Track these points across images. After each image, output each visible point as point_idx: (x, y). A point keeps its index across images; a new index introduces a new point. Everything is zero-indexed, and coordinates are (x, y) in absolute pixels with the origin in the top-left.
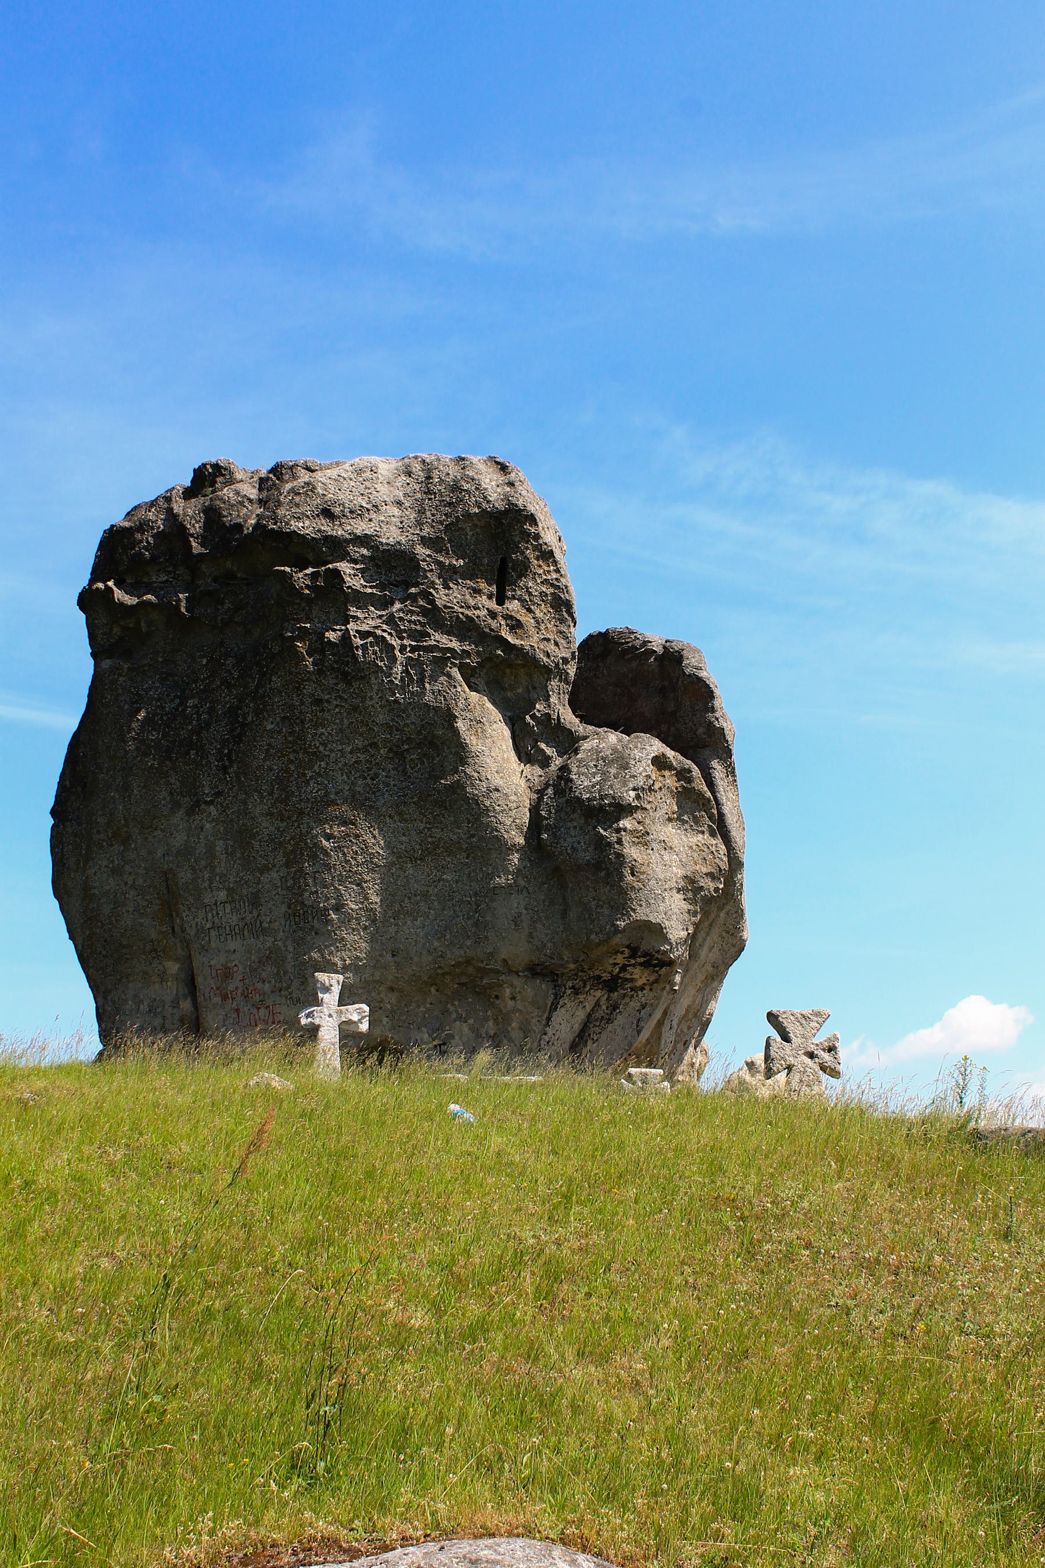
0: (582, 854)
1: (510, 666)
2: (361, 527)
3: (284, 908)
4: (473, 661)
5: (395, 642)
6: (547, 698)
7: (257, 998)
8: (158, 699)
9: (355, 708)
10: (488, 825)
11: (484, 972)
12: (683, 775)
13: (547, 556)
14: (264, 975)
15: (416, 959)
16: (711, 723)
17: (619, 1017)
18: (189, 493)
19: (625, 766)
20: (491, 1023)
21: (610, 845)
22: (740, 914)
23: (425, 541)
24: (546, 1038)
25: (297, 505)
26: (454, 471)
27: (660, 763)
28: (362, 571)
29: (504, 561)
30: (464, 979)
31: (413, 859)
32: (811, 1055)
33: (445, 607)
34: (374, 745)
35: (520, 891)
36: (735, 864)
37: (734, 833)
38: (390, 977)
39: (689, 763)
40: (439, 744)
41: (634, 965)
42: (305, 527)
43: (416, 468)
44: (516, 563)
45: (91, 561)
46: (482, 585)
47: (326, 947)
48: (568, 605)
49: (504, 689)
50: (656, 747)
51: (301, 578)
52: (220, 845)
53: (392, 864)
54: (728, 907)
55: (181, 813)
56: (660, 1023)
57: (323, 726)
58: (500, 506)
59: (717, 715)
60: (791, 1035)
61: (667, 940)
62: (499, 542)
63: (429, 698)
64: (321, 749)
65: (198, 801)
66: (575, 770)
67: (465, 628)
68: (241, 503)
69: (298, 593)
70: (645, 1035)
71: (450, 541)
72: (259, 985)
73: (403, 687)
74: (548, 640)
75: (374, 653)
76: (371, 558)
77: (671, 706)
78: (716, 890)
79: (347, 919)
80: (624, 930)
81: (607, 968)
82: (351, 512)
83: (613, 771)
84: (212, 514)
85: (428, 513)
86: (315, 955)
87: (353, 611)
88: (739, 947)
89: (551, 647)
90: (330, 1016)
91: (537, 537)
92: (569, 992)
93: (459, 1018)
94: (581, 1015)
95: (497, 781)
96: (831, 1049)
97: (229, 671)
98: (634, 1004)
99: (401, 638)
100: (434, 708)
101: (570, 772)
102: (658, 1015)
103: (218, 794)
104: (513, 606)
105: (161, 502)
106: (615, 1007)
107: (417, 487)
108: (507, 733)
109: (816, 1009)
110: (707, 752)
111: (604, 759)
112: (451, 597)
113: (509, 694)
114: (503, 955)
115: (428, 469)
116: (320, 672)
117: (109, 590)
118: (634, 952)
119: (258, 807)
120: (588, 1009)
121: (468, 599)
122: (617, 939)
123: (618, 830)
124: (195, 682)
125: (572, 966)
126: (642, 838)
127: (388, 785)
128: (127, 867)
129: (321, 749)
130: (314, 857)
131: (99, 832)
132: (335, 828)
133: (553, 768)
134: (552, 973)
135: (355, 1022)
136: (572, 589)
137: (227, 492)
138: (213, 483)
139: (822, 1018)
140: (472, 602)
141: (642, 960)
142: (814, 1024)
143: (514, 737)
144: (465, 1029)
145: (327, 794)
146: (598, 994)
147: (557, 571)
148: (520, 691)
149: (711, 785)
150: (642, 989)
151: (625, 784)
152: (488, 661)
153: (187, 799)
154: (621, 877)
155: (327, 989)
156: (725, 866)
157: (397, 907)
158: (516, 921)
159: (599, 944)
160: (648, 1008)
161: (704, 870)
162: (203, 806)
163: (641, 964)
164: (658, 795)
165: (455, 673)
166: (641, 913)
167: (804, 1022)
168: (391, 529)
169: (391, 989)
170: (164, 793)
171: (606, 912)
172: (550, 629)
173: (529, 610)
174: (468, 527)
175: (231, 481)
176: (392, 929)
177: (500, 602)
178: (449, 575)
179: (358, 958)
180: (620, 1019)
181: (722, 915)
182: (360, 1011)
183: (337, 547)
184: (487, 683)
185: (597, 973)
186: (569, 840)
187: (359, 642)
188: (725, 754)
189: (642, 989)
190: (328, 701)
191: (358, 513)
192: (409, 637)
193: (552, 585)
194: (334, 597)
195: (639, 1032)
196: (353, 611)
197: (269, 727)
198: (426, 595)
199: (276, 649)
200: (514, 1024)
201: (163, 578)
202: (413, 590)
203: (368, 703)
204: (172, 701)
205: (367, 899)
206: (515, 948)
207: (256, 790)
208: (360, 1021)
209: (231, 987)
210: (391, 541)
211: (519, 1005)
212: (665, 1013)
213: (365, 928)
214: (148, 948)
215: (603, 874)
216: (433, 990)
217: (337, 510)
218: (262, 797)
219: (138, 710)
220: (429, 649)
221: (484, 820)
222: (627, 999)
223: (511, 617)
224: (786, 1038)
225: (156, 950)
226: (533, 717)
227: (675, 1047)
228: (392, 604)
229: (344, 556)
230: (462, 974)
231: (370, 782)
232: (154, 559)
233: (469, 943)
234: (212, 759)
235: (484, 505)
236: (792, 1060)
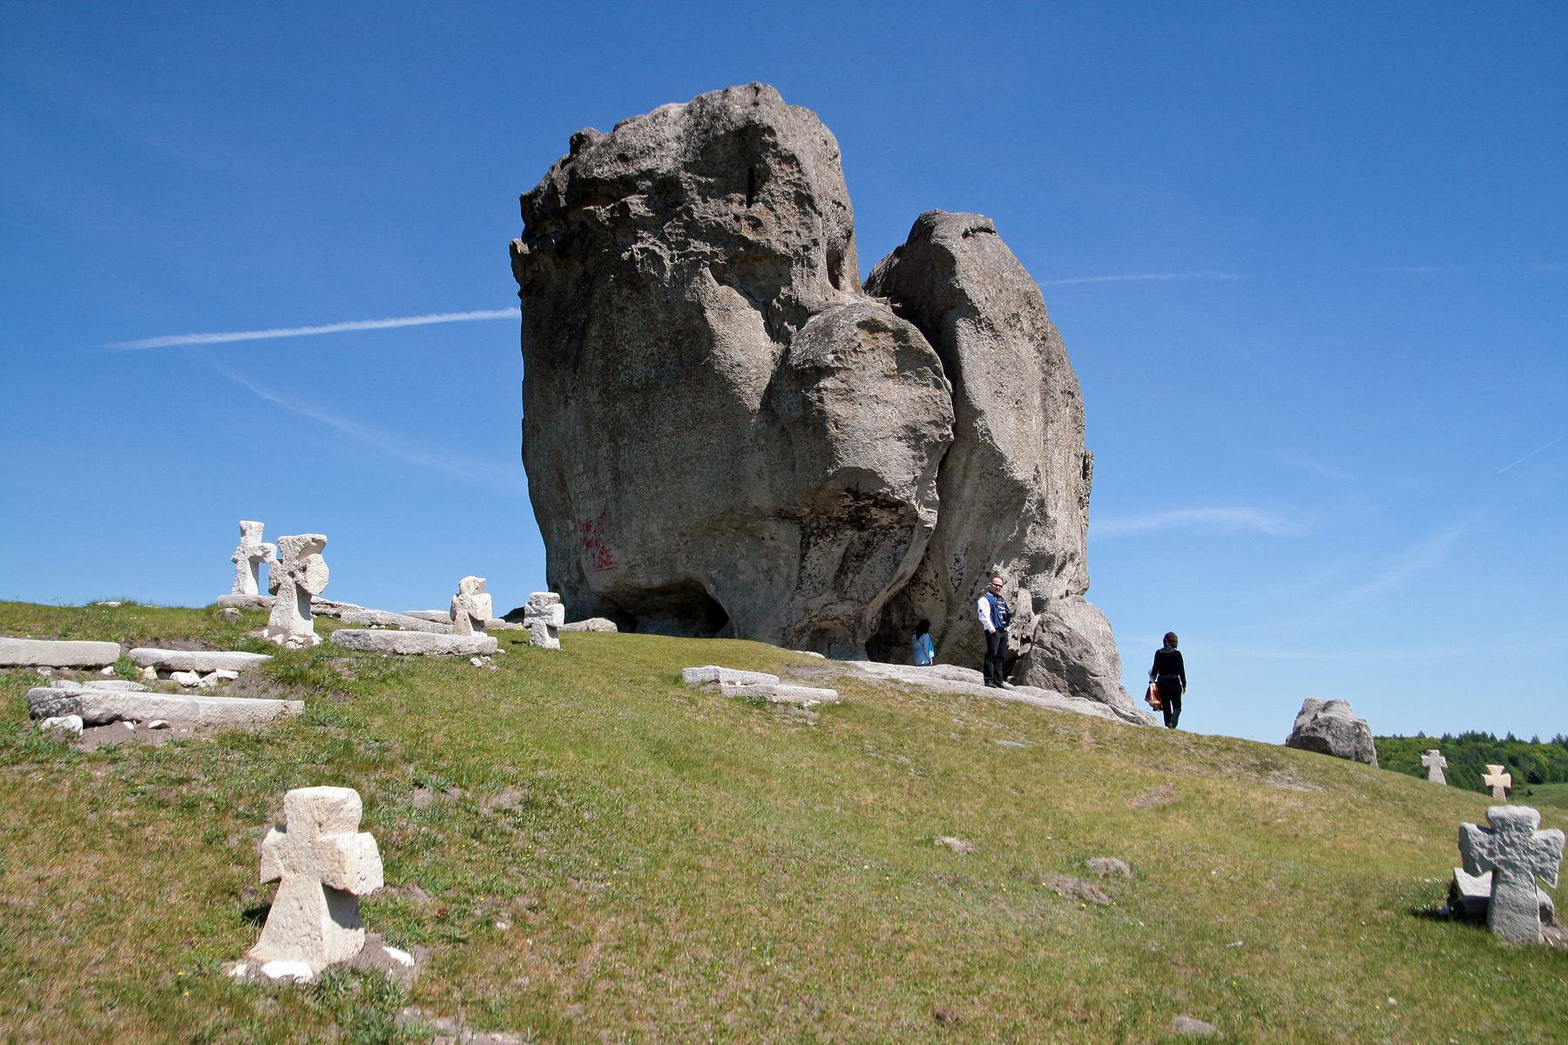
2: (646, 164)
6: (789, 283)
12: (900, 335)
13: (791, 159)
21: (811, 404)
23: (687, 167)
34: (660, 339)
42: (604, 171)
48: (810, 199)
51: (603, 213)
67: (716, 234)
69: (601, 225)
84: (572, 172)
91: (775, 145)
94: (838, 551)
95: (740, 357)
104: (758, 209)
112: (707, 210)
122: (831, 485)
123: (819, 390)
147: (800, 171)
154: (825, 430)
156: (949, 412)
158: (760, 474)
161: (927, 419)
164: (869, 356)
165: (707, 272)
166: (849, 461)
173: (772, 209)
174: (719, 148)
180: (879, 554)
183: (627, 185)
191: (646, 152)
194: (624, 223)
195: (897, 566)
206: (761, 497)
217: (630, 154)
223: (753, 218)
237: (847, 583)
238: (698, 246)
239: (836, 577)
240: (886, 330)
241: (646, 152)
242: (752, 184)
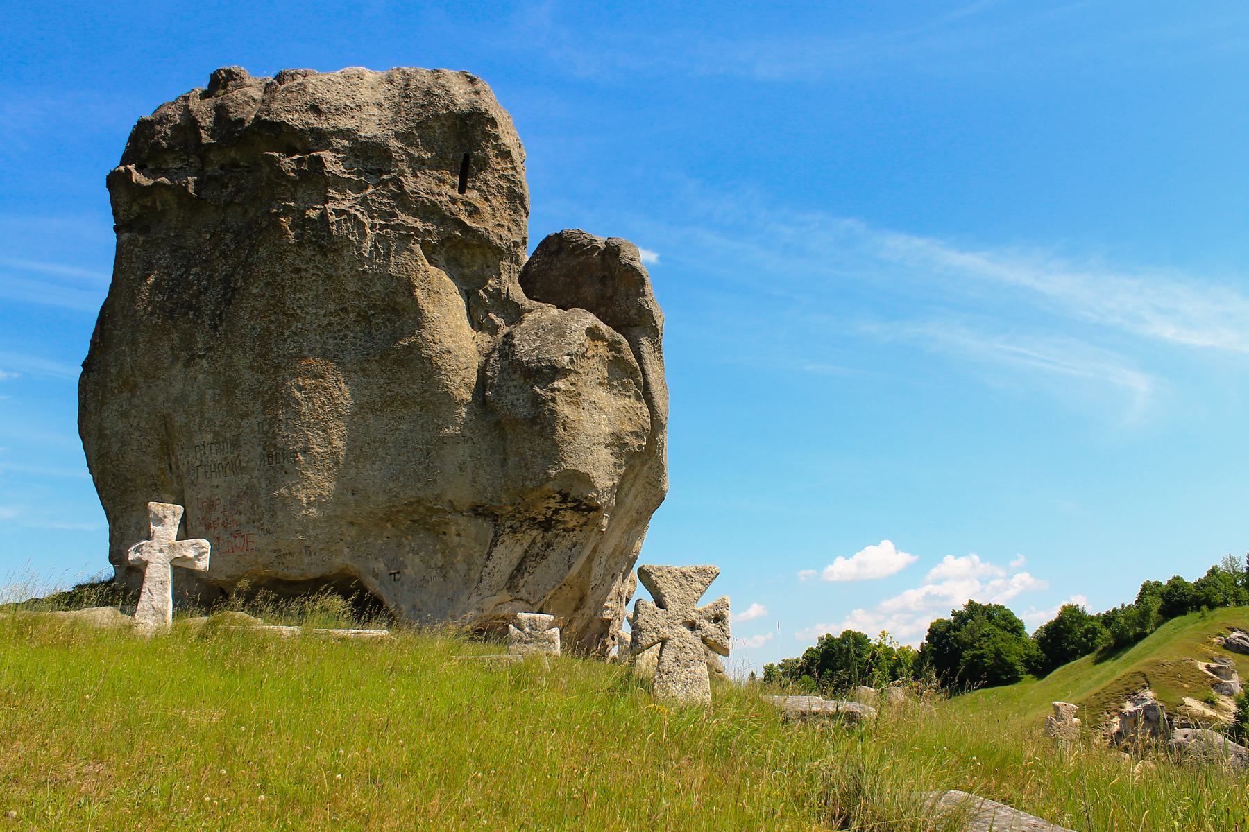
0: (520, 410)
1: (467, 246)
2: (344, 122)
3: (260, 449)
4: (433, 239)
5: (367, 221)
7: (235, 528)
8: (166, 267)
9: (329, 277)
10: (439, 382)
12: (613, 346)
13: (506, 155)
14: (241, 508)
15: (373, 498)
16: (641, 305)
17: (553, 554)
18: (205, 95)
19: (562, 335)
20: (439, 556)
21: (544, 402)
22: (660, 469)
23: (398, 136)
24: (487, 570)
25: (289, 101)
26: (429, 80)
27: (593, 333)
28: (343, 159)
29: (467, 158)
30: (415, 517)
31: (373, 410)
32: (692, 626)
33: (413, 192)
34: (344, 310)
35: (466, 441)
36: (657, 425)
37: (658, 399)
38: (350, 513)
39: (619, 336)
40: (399, 310)
41: (565, 510)
42: (296, 119)
43: (398, 77)
44: (477, 159)
45: (122, 149)
46: (447, 176)
47: (294, 485)
48: (522, 198)
49: (462, 267)
50: (591, 320)
51: (288, 163)
53: (355, 414)
54: (651, 462)
55: (179, 365)
56: (590, 559)
57: (301, 291)
58: (466, 109)
59: (647, 299)
60: (667, 599)
61: (594, 489)
62: (463, 141)
63: (393, 269)
64: (299, 311)
65: (193, 355)
66: (518, 336)
67: (429, 211)
68: (247, 103)
69: (284, 176)
70: (575, 570)
71: (420, 137)
72: (237, 517)
73: (371, 260)
74: (502, 226)
75: (347, 229)
76: (352, 149)
77: (609, 292)
78: (640, 446)
79: (313, 461)
80: (555, 478)
81: (541, 511)
82: (337, 109)
83: (551, 338)
84: (221, 111)
85: (403, 114)
86: (284, 492)
87: (332, 192)
88: (658, 498)
89: (504, 232)
90: (161, 551)
91: (497, 138)
92: (507, 530)
93: (412, 550)
94: (519, 551)
95: (450, 344)
96: (718, 619)
97: (227, 245)
98: (566, 543)
99: (373, 218)
100: (397, 279)
101: (513, 338)
102: (587, 552)
103: (209, 349)
104: (472, 195)
105: (181, 101)
106: (549, 545)
107: (397, 92)
108: (462, 303)
109: (701, 565)
110: (637, 331)
112: (419, 184)
113: (466, 271)
114: (450, 496)
115: (407, 78)
116: (300, 245)
117: (129, 172)
118: (565, 497)
119: (242, 361)
121: (434, 186)
123: (553, 390)
124: (199, 253)
125: (510, 508)
126: (574, 398)
127: (355, 345)
128: (133, 411)
129: (299, 311)
130: (288, 405)
131: (111, 381)
132: (307, 381)
133: (501, 335)
134: (492, 513)
135: (190, 559)
136: (526, 185)
137: (237, 94)
138: (225, 87)
139: (707, 576)
140: (436, 190)
141: (572, 505)
142: (697, 585)
143: (468, 307)
144: (417, 560)
145: (301, 351)
146: (534, 533)
147: (514, 168)
148: (475, 268)
149: (639, 358)
151: (560, 350)
152: (447, 240)
153: (184, 353)
154: (554, 431)
155: (160, 521)
156: (648, 426)
157: (358, 451)
159: (532, 490)
160: (578, 547)
161: (630, 429)
162: (197, 360)
163: (572, 509)
164: (591, 362)
165: (418, 249)
166: (571, 464)
167: (684, 582)
168: (370, 127)
169: (352, 524)
170: (166, 348)
171: (540, 461)
172: (505, 217)
173: (487, 200)
174: (436, 125)
175: (241, 85)
176: (353, 471)
177: (462, 190)
178: (418, 165)
179: (321, 495)
181: (645, 469)
182: (198, 547)
183: (322, 138)
184: (447, 261)
185: (533, 515)
186: (510, 397)
187: (334, 219)
188: (654, 333)
189: (573, 530)
190: (306, 270)
191: (343, 111)
192: (380, 217)
193: (508, 180)
195: (570, 567)
196: (332, 192)
197: (254, 291)
198: (398, 183)
199: (264, 224)
200: (459, 558)
202: (385, 177)
204: (179, 269)
205: (331, 443)
206: (460, 491)
207: (240, 346)
208: (197, 557)
209: (214, 518)
210: (369, 135)
211: (464, 541)
212: (595, 550)
213: (329, 469)
214: (149, 482)
216: (389, 525)
217: (323, 107)
218: (245, 352)
219: (149, 276)
220: (394, 227)
221: (437, 377)
222: (560, 539)
223: (470, 204)
224: (661, 604)
225: (155, 484)
226: (486, 291)
227: (603, 579)
228: (367, 188)
229: (328, 146)
230: (414, 512)
231: (339, 341)
232: (170, 148)
233: (419, 485)
235: (452, 107)
236: (666, 632)
237: (521, 583)
238: (405, 219)
239: (512, 577)
240: (603, 339)
241: (343, 111)
242: (467, 171)
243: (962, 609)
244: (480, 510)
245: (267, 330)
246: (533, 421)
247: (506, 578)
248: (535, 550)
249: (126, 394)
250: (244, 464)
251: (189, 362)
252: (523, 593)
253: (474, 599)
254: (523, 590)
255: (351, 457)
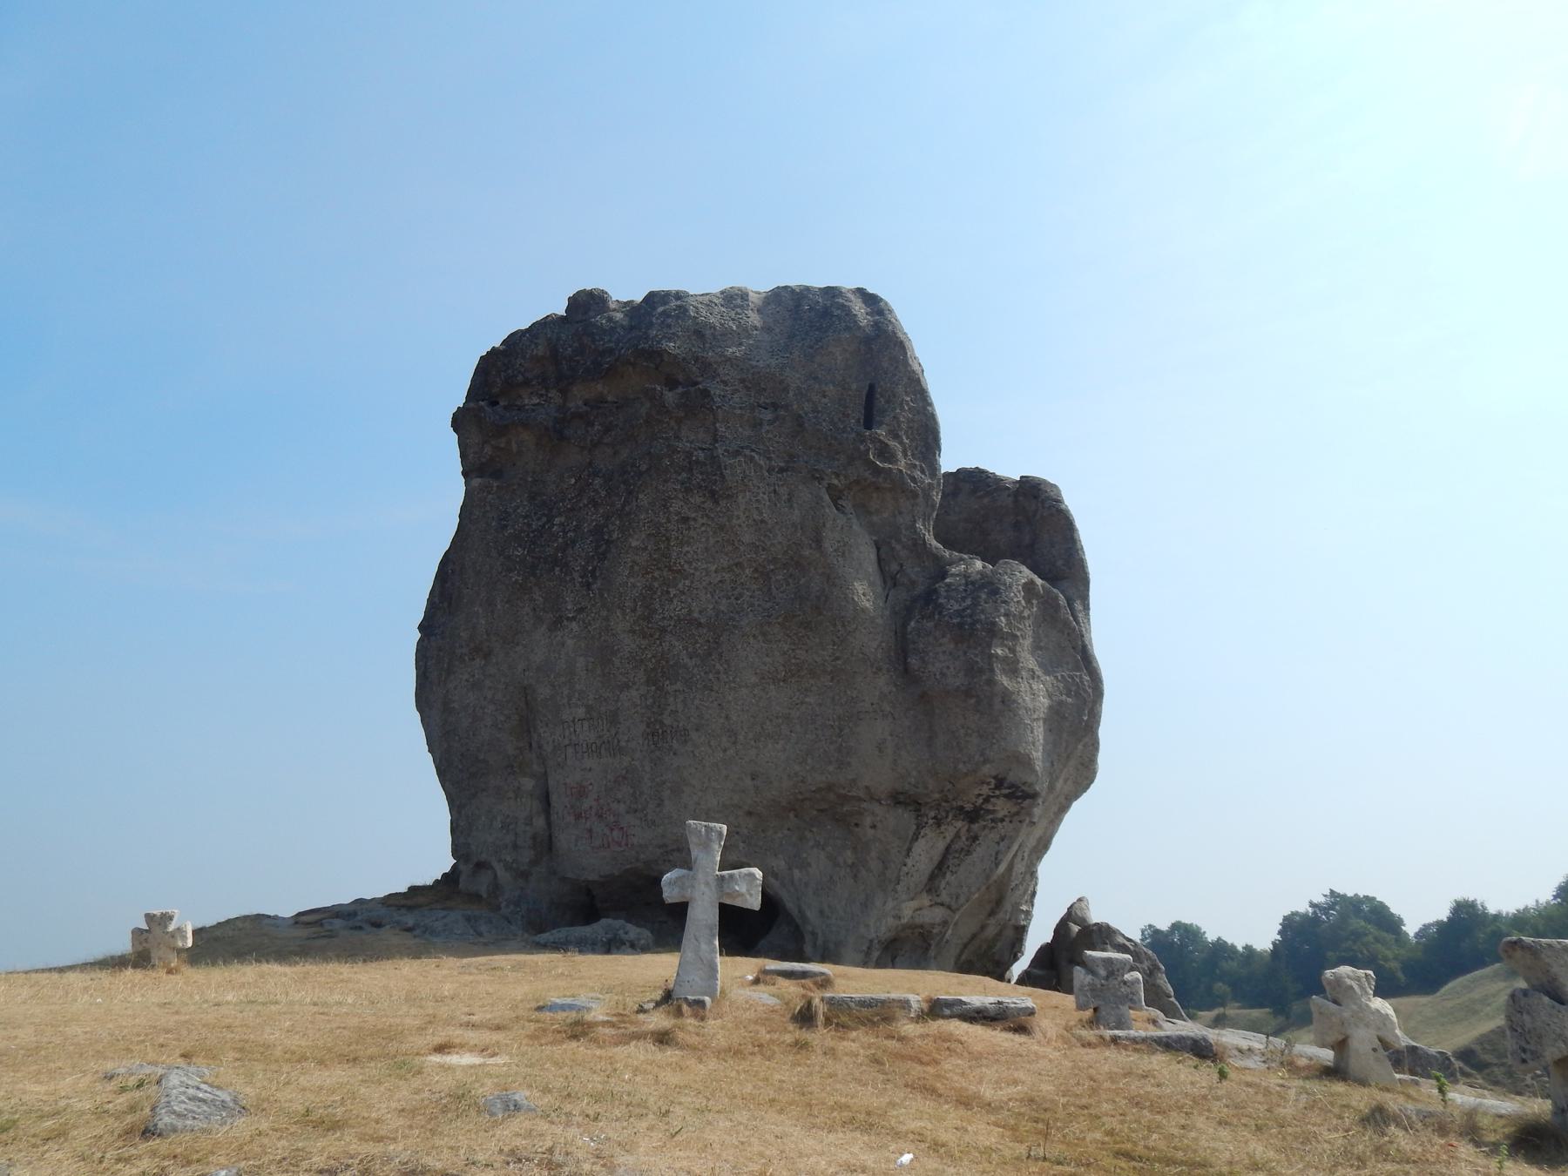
3: (643, 727)
7: (612, 819)
8: (526, 517)
9: (722, 528)
11: (845, 799)
19: (995, 592)
20: (849, 853)
25: (669, 326)
50: (1025, 574)
52: (581, 662)
57: (689, 544)
70: (1002, 868)
72: (614, 806)
89: (917, 474)
94: (941, 846)
99: (770, 459)
103: (581, 610)
106: (975, 838)
111: (973, 583)
113: (875, 519)
118: (1000, 783)
120: (948, 840)
124: (563, 500)
125: (937, 796)
126: (1013, 669)
127: (752, 605)
145: (690, 612)
146: (959, 824)
150: (1002, 820)
158: (880, 748)
169: (749, 813)
189: (1002, 820)
195: (997, 865)
197: (634, 544)
199: (644, 467)
201: (536, 400)
203: (734, 521)
215: (973, 701)
216: (792, 815)
218: (624, 614)
233: (831, 768)
234: (576, 575)
237: (943, 884)
239: (933, 877)
243: (1323, 900)
244: (902, 798)
245: (650, 588)
246: (968, 693)
247: (925, 878)
248: (956, 846)
249: (479, 662)
250: (623, 744)
251: (557, 624)
252: (944, 897)
253: (890, 904)
254: (944, 893)
255: (751, 735)
